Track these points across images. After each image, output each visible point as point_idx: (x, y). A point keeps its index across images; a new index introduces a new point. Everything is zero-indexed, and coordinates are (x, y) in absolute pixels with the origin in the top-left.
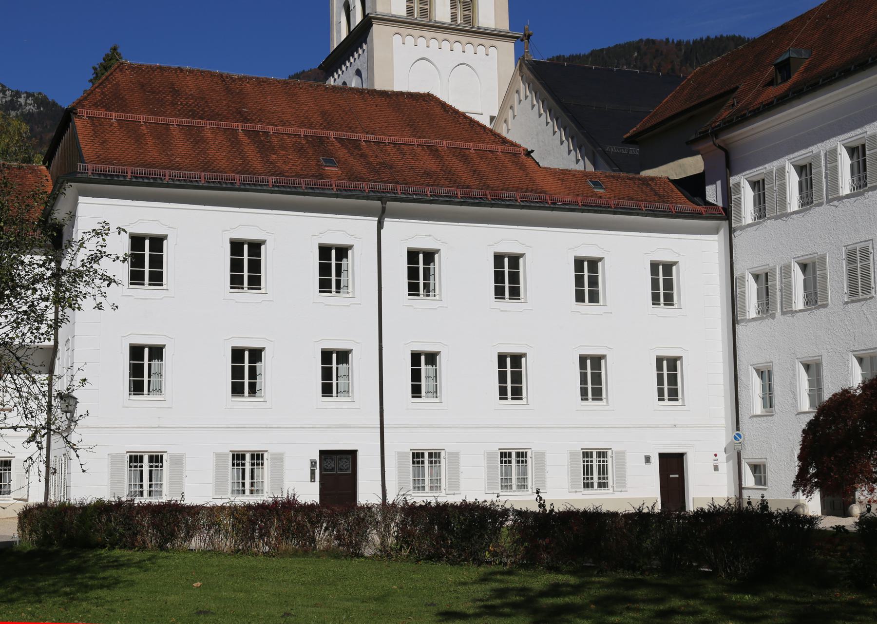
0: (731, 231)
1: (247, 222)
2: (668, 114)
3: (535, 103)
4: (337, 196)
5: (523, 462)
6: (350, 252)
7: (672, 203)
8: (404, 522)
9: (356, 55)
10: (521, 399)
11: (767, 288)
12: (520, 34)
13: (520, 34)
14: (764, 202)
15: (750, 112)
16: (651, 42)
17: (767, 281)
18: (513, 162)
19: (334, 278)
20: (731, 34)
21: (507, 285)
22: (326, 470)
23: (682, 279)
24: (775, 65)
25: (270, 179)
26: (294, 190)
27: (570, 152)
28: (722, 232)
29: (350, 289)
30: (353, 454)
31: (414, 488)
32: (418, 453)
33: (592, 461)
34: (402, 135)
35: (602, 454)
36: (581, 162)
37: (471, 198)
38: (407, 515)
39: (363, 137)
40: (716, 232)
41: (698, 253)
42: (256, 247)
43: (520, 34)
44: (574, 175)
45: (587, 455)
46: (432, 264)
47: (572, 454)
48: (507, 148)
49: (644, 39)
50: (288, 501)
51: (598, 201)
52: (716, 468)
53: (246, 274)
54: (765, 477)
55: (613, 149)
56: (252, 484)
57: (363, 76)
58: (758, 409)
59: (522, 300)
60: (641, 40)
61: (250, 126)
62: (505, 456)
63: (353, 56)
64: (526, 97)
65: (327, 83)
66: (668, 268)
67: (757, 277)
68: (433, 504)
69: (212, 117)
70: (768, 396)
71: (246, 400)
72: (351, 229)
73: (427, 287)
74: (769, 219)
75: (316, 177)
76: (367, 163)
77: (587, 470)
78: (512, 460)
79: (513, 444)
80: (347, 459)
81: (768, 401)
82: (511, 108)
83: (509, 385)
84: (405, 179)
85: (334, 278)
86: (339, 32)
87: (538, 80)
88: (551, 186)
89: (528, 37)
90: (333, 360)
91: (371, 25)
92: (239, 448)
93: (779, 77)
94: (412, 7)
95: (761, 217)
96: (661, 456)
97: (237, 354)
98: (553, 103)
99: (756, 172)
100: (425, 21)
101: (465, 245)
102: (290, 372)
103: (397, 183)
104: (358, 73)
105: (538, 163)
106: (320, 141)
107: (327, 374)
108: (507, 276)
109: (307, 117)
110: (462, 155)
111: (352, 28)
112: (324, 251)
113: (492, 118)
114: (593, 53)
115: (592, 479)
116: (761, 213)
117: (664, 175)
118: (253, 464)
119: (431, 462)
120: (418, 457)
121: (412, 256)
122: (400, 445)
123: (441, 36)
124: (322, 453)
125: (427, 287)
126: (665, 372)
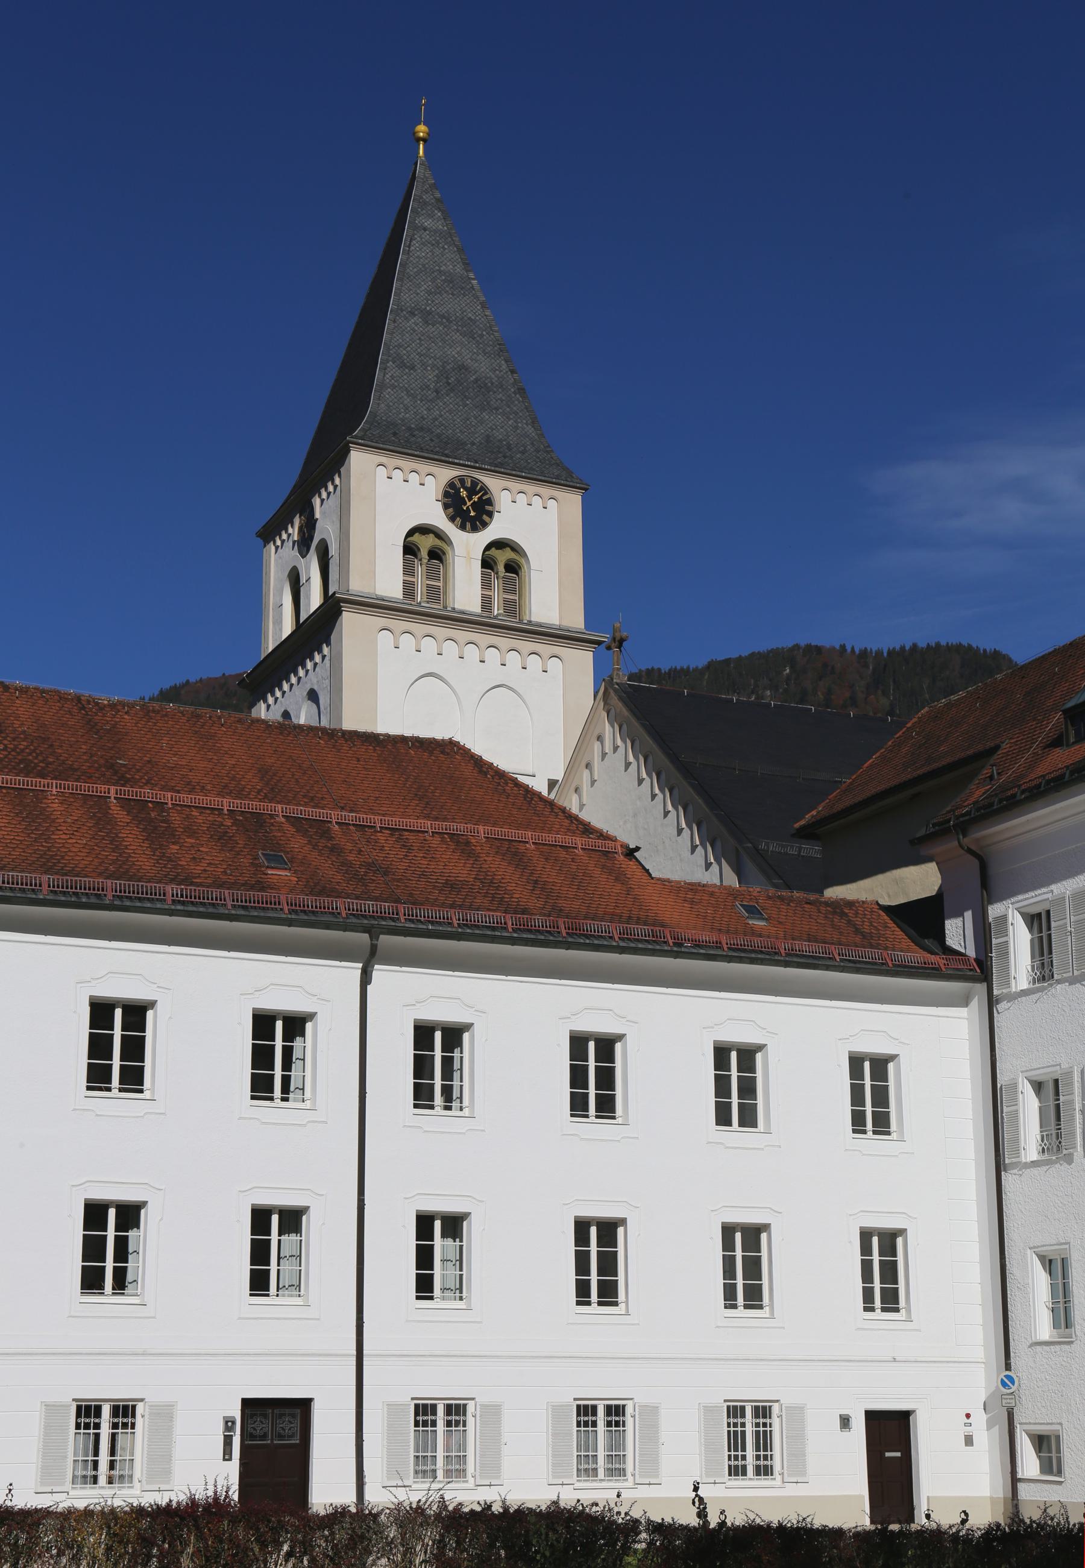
0: (992, 1002)
1: (123, 967)
2: (872, 790)
3: (631, 758)
4: (290, 923)
5: (617, 1424)
6: (309, 1026)
7: (886, 948)
8: (441, 1544)
9: (309, 665)
10: (616, 1304)
11: (1058, 1107)
12: (605, 637)
13: (603, 633)
14: (1050, 952)
15: (1023, 792)
16: (814, 651)
17: (1057, 1093)
18: (604, 867)
19: (278, 1072)
20: (954, 640)
21: (592, 1091)
22: (252, 1437)
23: (908, 1088)
24: (1065, 712)
25: (169, 889)
26: (211, 910)
27: (694, 848)
28: (975, 1003)
29: (308, 1093)
30: (303, 1406)
31: (416, 1472)
32: (425, 1406)
33: (743, 1425)
34: (404, 815)
35: (762, 1412)
36: (715, 868)
37: (530, 931)
38: (447, 1529)
39: (335, 816)
40: (964, 1002)
41: (932, 1040)
42: (137, 1014)
43: (605, 637)
44: (712, 894)
45: (735, 1411)
46: (457, 1051)
47: (708, 1410)
48: (592, 841)
49: (803, 643)
50: (216, 1499)
51: (757, 941)
52: (969, 1441)
53: (116, 1063)
54: (1059, 1460)
55: (773, 847)
56: (112, 1465)
57: (321, 702)
58: (1044, 1329)
59: (619, 1120)
60: (797, 647)
61: (131, 792)
62: (586, 1412)
63: (304, 666)
64: (616, 749)
65: (254, 713)
66: (880, 1065)
67: (1038, 1087)
68: (497, 1508)
69: (61, 774)
70: (1061, 1305)
71: (107, 1300)
72: (314, 984)
73: (447, 1092)
74: (1059, 982)
75: (252, 888)
76: (343, 864)
77: (736, 1441)
78: (600, 1420)
79: (601, 1389)
80: (293, 1416)
81: (1063, 1314)
82: (588, 766)
83: (594, 1278)
84: (411, 895)
85: (278, 1072)
86: (279, 622)
87: (638, 719)
88: (672, 913)
89: (620, 643)
90: (273, 1227)
91: (339, 613)
92: (90, 1393)
93: (1072, 733)
94: (413, 583)
95: (1043, 979)
96: (872, 1416)
97: (95, 1213)
98: (665, 762)
99: (1036, 898)
100: (435, 608)
101: (520, 1018)
102: (191, 1250)
103: (398, 901)
104: (313, 696)
105: (647, 871)
106: (259, 821)
107: (260, 1253)
108: (594, 1075)
109: (233, 778)
110: (511, 852)
111: (303, 617)
112: (263, 1023)
113: (552, 784)
114: (711, 666)
115: (744, 1458)
116: (1045, 969)
117: (870, 898)
118: (115, 1426)
119: (449, 1424)
120: (424, 1412)
121: (423, 1033)
122: (393, 1389)
123: (463, 635)
124: (247, 1403)
125: (447, 1092)
126: (876, 1258)
